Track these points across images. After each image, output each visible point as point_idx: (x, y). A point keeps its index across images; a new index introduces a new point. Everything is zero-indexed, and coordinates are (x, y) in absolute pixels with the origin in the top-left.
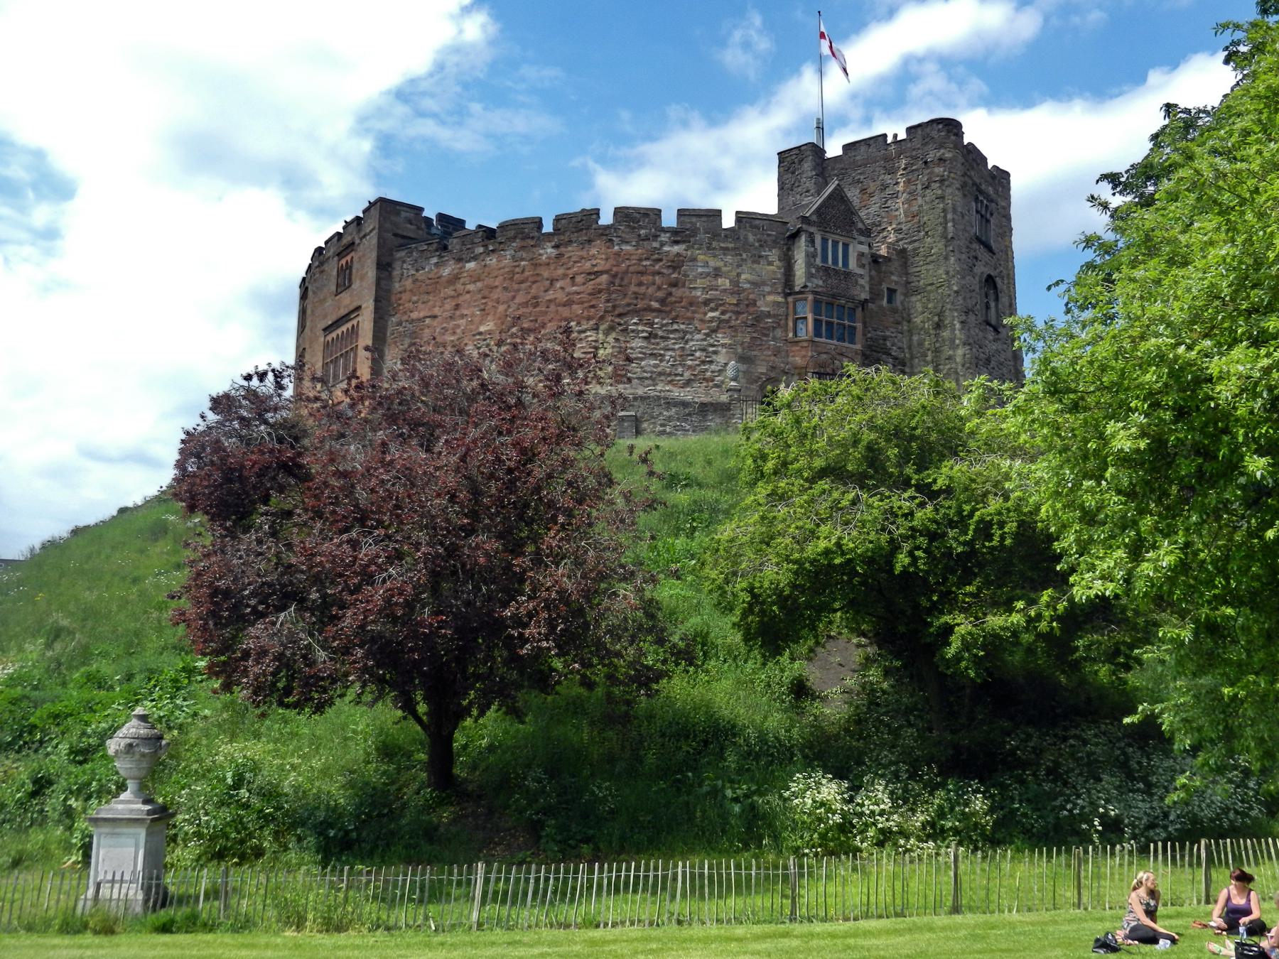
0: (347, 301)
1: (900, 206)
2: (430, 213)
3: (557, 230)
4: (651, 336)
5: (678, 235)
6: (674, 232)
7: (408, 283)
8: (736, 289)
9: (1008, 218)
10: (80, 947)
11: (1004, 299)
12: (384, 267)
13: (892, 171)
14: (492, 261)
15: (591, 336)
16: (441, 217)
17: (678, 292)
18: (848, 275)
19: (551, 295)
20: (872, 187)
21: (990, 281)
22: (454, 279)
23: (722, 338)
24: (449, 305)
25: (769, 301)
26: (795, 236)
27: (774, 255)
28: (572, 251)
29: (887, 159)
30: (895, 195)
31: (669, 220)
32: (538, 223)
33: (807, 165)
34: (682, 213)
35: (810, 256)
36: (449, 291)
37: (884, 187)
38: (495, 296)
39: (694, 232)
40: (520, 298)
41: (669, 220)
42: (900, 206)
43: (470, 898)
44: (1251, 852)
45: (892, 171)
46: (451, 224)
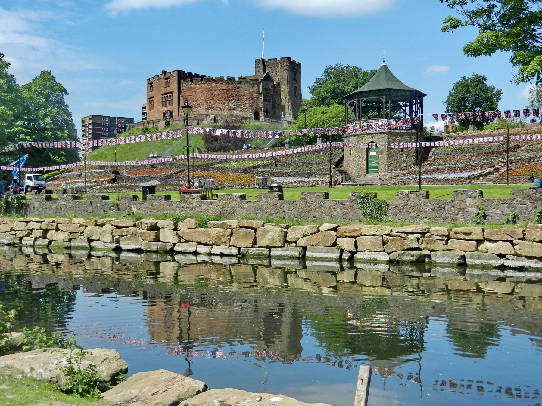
0: (168, 90)
1: (279, 73)
2: (186, 72)
5: (239, 82)
6: (238, 82)
8: (250, 93)
9: (300, 73)
10: (464, 137)
11: (299, 90)
13: (277, 66)
14: (203, 85)
15: (223, 102)
16: (188, 73)
18: (269, 90)
19: (215, 93)
20: (274, 69)
21: (296, 87)
22: (195, 88)
23: (247, 102)
24: (194, 93)
25: (255, 95)
26: (260, 83)
27: (256, 86)
28: (219, 85)
29: (277, 64)
30: (278, 71)
31: (237, 79)
33: (261, 63)
35: (263, 87)
36: (194, 90)
37: (276, 69)
38: (204, 92)
39: (242, 81)
40: (209, 93)
41: (237, 79)
42: (279, 73)
46: (190, 74)
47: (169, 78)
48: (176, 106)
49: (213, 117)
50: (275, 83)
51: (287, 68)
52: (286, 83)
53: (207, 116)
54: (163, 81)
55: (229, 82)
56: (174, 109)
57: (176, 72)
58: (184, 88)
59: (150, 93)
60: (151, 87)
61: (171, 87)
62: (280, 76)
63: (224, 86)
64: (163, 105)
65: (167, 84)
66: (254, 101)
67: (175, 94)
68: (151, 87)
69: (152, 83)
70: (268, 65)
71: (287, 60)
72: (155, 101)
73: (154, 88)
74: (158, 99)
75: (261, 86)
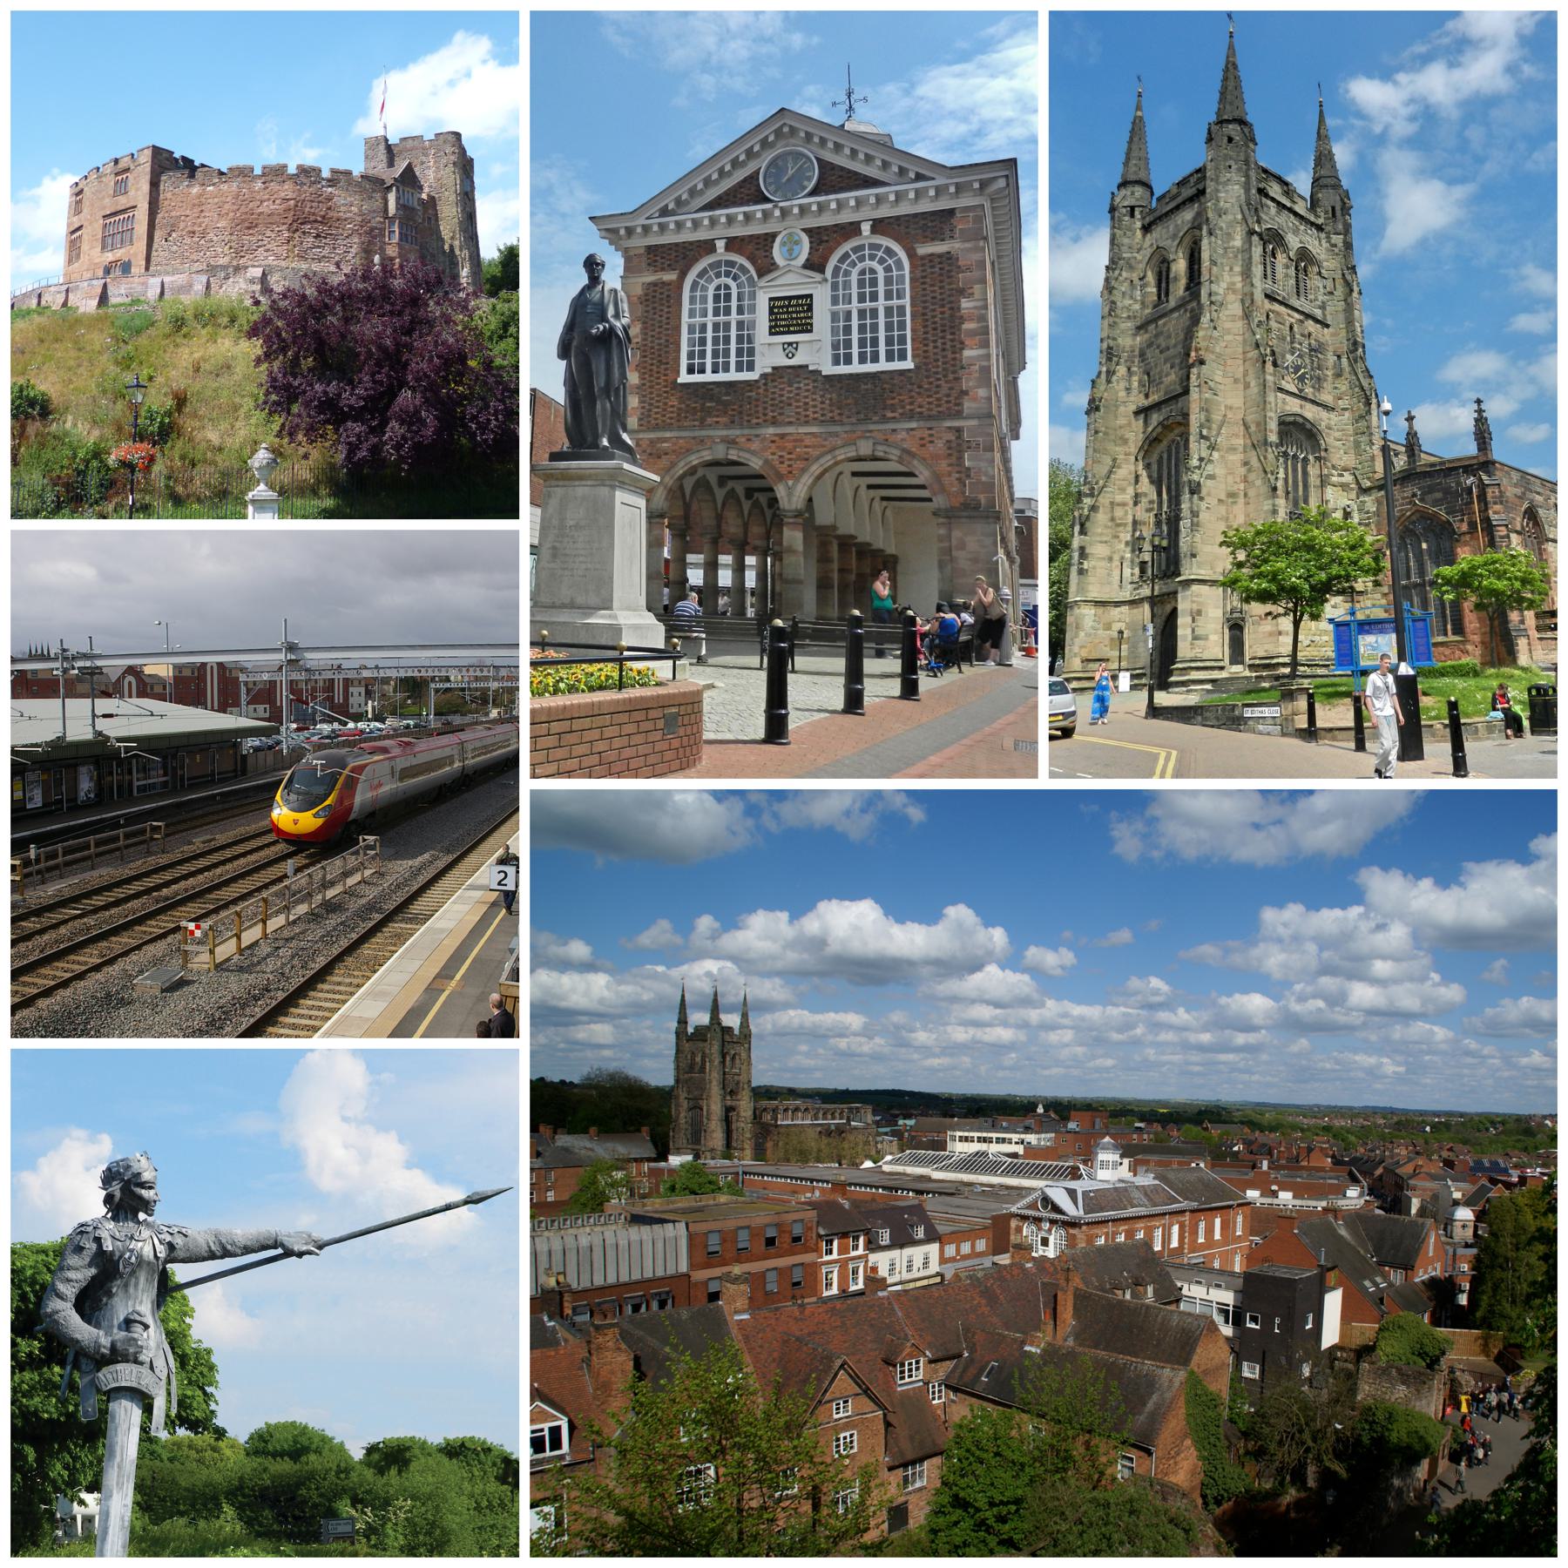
0: (123, 202)
2: (177, 155)
3: (264, 175)
4: (318, 236)
5: (332, 182)
7: (169, 195)
12: (155, 184)
13: (426, 155)
14: (224, 187)
16: (184, 158)
17: (331, 214)
26: (389, 189)
27: (378, 195)
31: (326, 174)
32: (252, 169)
34: (333, 171)
35: (398, 199)
40: (243, 209)
43: (1084, 1193)
44: (78, 855)
45: (426, 155)
46: (1476, 420)
47: (127, 170)
48: (141, 245)
49: (258, 272)
50: (424, 196)
51: (453, 158)
52: (453, 198)
53: (237, 269)
54: (110, 181)
55: (303, 178)
56: (135, 255)
57: (148, 153)
58: (169, 195)
59: (75, 219)
60: (79, 202)
61: (132, 193)
62: (435, 177)
63: (288, 190)
64: (103, 248)
65: (121, 188)
66: (374, 237)
67: (142, 214)
68: (79, 202)
69: (81, 191)
70: (401, 152)
71: (450, 138)
72: (85, 237)
73: (86, 203)
74: (93, 230)
75: (392, 197)
